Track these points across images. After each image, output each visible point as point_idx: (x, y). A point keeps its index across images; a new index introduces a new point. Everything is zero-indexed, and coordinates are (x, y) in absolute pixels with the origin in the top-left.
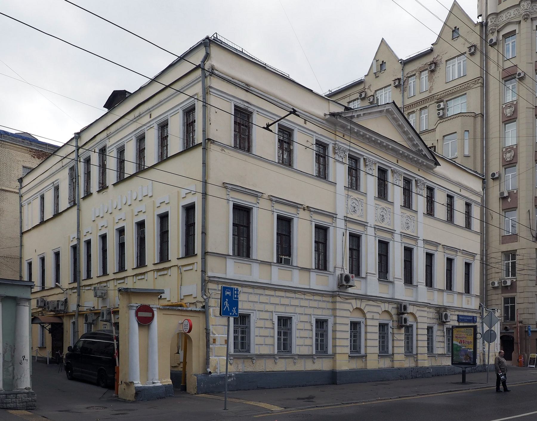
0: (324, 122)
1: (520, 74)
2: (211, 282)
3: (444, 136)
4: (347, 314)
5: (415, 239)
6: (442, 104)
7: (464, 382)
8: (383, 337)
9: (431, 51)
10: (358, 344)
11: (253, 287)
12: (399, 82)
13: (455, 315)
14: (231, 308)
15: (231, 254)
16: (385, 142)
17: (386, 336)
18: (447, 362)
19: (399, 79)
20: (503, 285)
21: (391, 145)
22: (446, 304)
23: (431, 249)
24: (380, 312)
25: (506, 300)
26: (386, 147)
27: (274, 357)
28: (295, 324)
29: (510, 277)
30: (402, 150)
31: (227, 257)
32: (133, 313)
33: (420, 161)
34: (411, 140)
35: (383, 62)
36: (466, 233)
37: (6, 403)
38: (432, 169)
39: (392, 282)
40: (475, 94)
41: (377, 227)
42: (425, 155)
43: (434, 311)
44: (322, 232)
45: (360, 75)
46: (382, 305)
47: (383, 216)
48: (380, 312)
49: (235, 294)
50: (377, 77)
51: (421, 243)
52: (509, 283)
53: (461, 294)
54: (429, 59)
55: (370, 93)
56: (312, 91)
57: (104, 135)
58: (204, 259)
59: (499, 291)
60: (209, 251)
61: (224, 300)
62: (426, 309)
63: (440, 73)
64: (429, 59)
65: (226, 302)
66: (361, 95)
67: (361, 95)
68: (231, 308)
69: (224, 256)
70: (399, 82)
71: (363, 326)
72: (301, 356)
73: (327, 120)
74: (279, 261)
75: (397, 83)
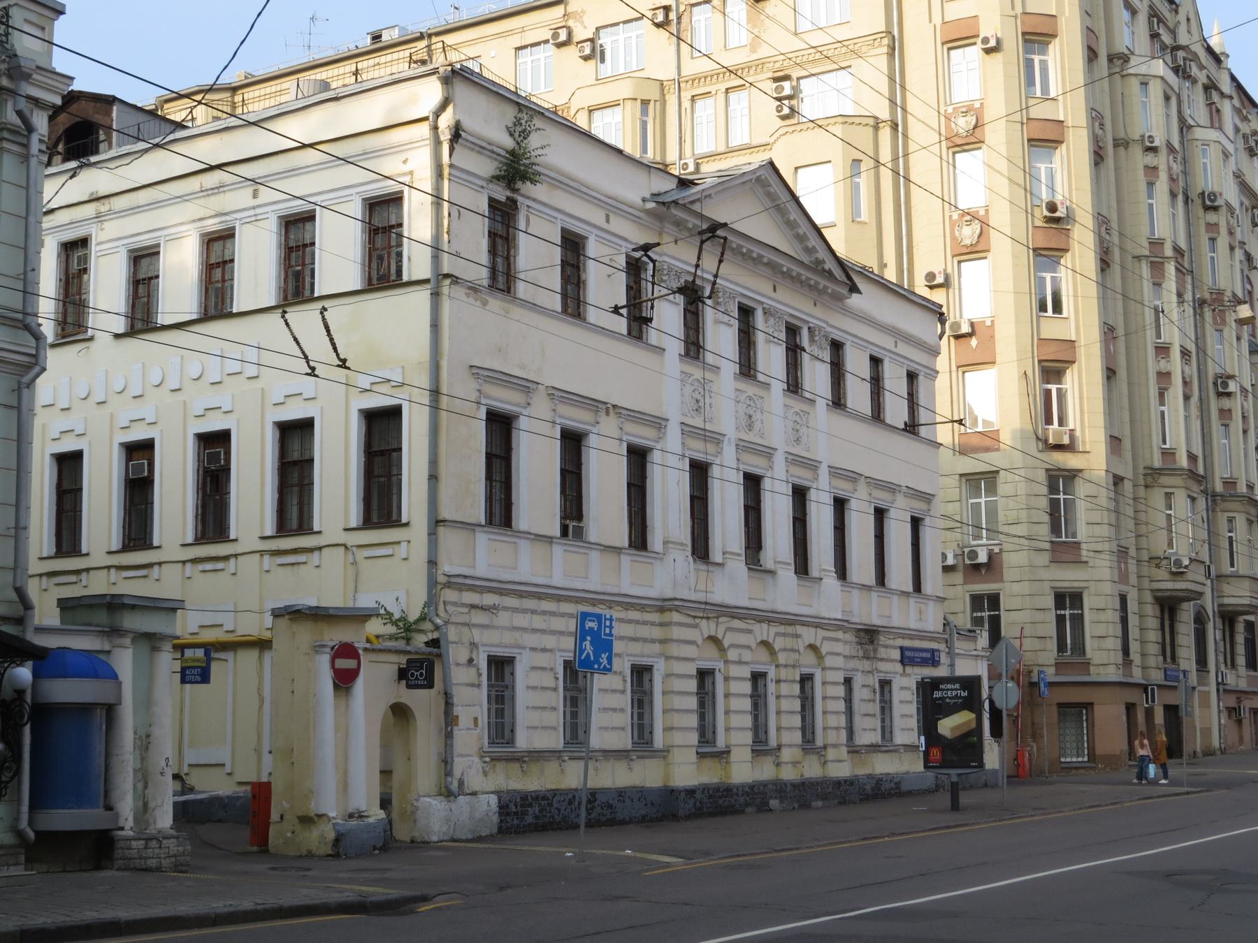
0: (642, 215)
1: (985, 41)
2: (448, 585)
3: (796, 169)
4: (690, 651)
5: (812, 465)
6: (786, 85)
7: (955, 806)
8: (640, 704)
10: (646, 721)
11: (521, 595)
12: (667, 16)
13: (895, 648)
14: (597, 656)
15: (483, 522)
16: (757, 250)
17: (646, 700)
18: (913, 765)
19: (667, 9)
20: (967, 562)
21: (768, 256)
22: (876, 621)
23: (843, 489)
24: (754, 646)
25: (977, 601)
26: (757, 260)
27: (559, 758)
28: (522, 676)
29: (984, 541)
30: (786, 265)
31: (478, 529)
32: (324, 660)
33: (821, 287)
34: (801, 238)
37: (146, 858)
38: (838, 298)
39: (772, 573)
40: (874, 68)
41: (742, 444)
42: (830, 273)
43: (854, 639)
44: (638, 457)
46: (757, 627)
47: (750, 416)
48: (754, 646)
51: (824, 472)
52: (982, 558)
53: (905, 594)
56: (620, 152)
57: (89, 210)
58: (432, 534)
59: (958, 577)
60: (447, 517)
61: (583, 639)
62: (840, 635)
65: (588, 643)
66: (556, 35)
67: (556, 35)
68: (597, 656)
69: (470, 527)
70: (667, 16)
71: (719, 679)
72: (609, 754)
73: (648, 212)
74: (564, 532)
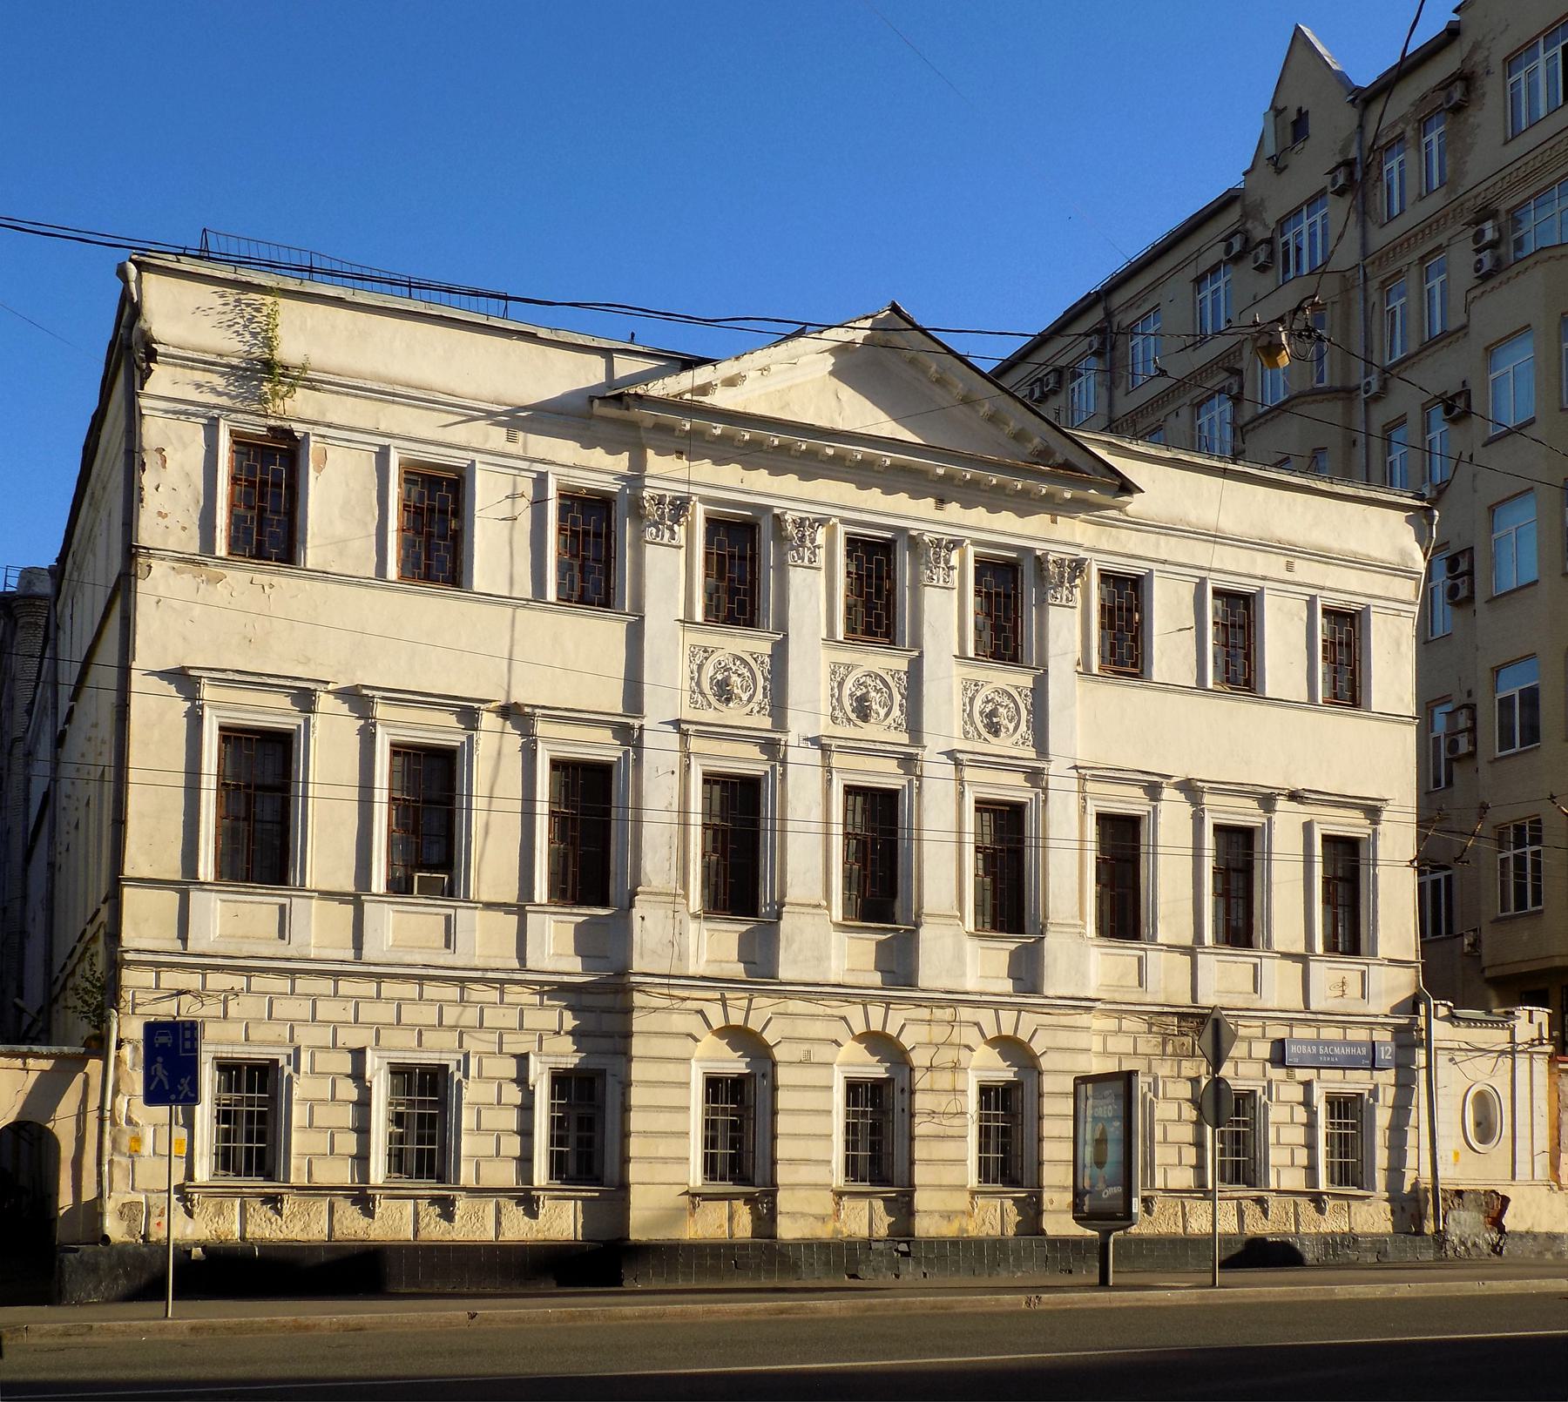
9: (1453, 33)
19: (1348, 164)
35: (1300, 110)
36: (1342, 725)
43: (570, 1022)
45: (1233, 179)
49: (185, 1040)
50: (1279, 171)
54: (1448, 63)
55: (1260, 233)
63: (1488, 115)
64: (1448, 63)
65: (159, 1066)
75: (1341, 181)
